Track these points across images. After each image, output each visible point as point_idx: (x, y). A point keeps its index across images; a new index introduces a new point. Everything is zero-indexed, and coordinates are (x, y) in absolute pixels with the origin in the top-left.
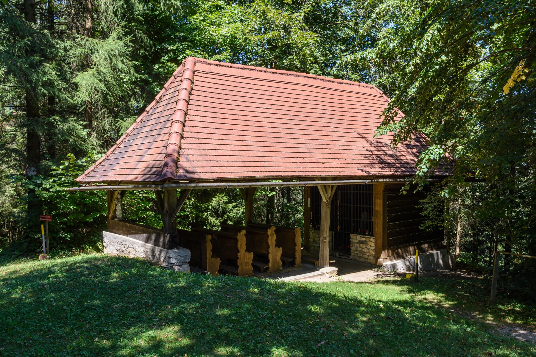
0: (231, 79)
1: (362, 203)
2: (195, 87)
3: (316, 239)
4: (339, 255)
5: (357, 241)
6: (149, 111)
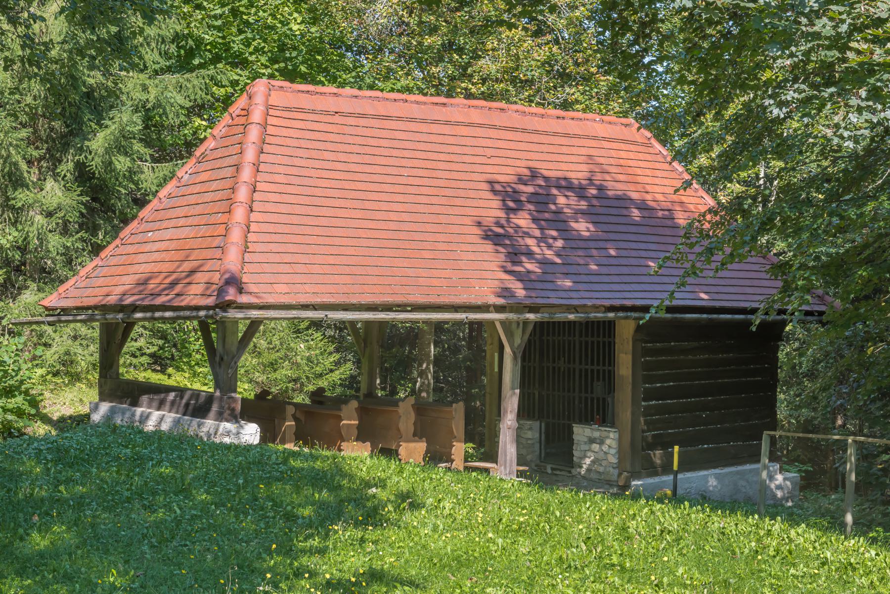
0: (337, 119)
2: (268, 139)
4: (552, 469)
6: (182, 177)
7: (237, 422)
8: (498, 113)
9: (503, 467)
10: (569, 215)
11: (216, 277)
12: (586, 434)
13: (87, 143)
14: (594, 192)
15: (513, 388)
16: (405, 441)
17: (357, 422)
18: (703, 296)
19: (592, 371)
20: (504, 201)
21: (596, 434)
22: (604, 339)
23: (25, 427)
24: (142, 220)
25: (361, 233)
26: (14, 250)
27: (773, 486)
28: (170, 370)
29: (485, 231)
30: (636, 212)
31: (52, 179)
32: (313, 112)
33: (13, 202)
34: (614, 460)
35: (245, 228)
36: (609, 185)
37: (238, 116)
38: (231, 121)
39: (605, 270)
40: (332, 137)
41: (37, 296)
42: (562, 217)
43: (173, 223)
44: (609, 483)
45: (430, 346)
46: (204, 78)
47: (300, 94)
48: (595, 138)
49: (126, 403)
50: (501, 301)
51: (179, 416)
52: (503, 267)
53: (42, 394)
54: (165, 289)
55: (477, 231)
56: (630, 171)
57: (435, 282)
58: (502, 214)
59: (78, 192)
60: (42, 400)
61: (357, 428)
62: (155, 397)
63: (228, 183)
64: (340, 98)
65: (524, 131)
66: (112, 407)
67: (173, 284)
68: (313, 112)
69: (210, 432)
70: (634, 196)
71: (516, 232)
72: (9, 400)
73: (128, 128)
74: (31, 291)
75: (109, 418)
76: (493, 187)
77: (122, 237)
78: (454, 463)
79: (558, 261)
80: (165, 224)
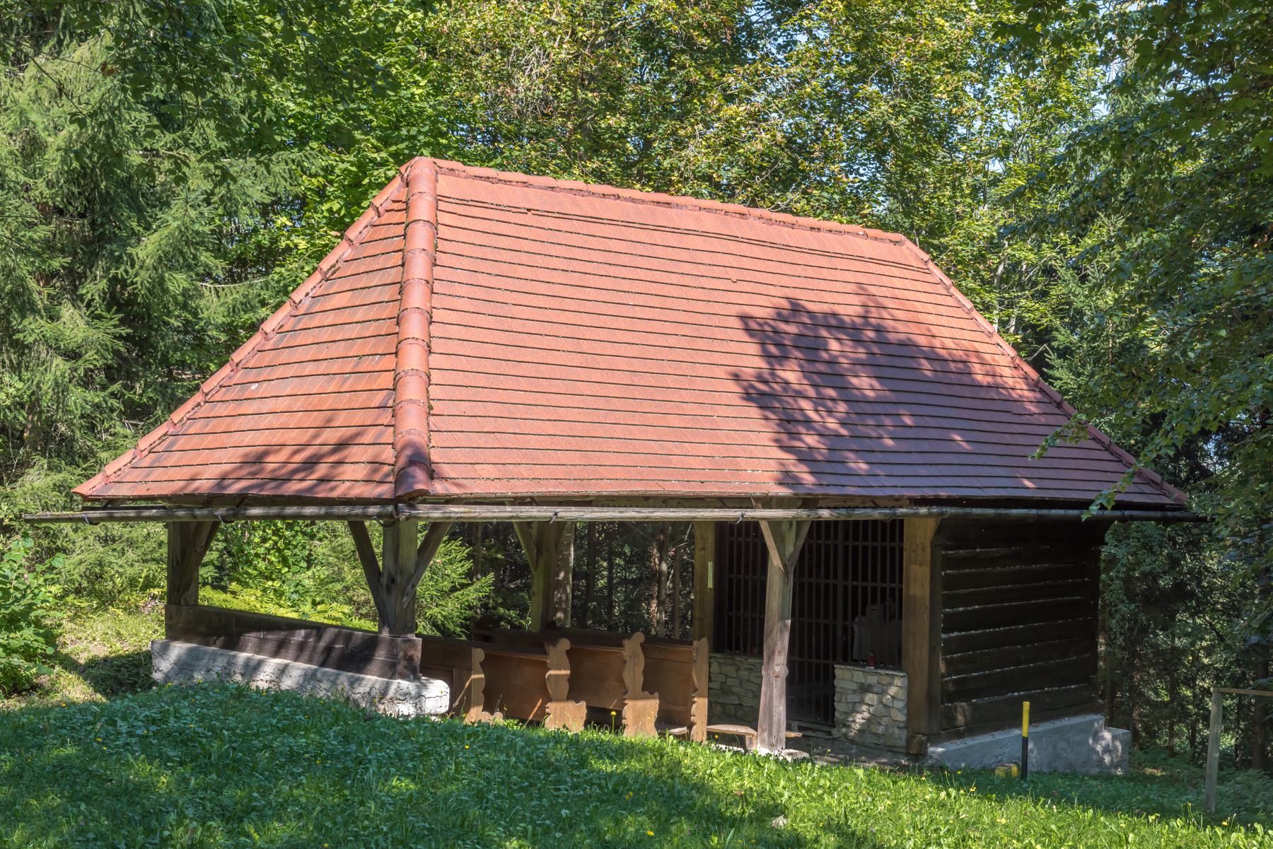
0: (529, 219)
1: (831, 587)
2: (442, 246)
3: (730, 682)
5: (855, 687)
6: (300, 302)
7: (417, 678)
8: (737, 219)
9: (766, 734)
10: (846, 366)
11: (388, 454)
12: (855, 679)
13: (129, 250)
14: (871, 334)
15: (782, 618)
16: (631, 699)
17: (568, 672)
18: (1028, 483)
19: (865, 589)
20: (763, 344)
21: (872, 680)
22: (884, 544)
23: (38, 675)
24: (237, 365)
25: (581, 388)
26: (15, 409)
27: (1099, 748)
28: (234, 586)
29: (745, 388)
30: (925, 364)
31: (70, 305)
32: (498, 207)
33: (20, 336)
34: (901, 717)
35: (425, 377)
36: (889, 324)
37: (387, 211)
38: (376, 218)
39: (904, 446)
40: (525, 246)
41: (49, 478)
42: (838, 369)
43: (292, 370)
44: (892, 750)
45: (569, 550)
46: (287, 164)
47: (477, 182)
48: (860, 258)
49: (214, 644)
50: (783, 491)
51: (314, 667)
52: (777, 441)
53: (60, 625)
54: (296, 471)
55: (733, 386)
56: (909, 305)
57: (694, 462)
58: (762, 364)
59: (115, 322)
60: (61, 634)
61: (569, 680)
62: (269, 637)
63: (390, 310)
64: (530, 190)
65: (773, 245)
66: (191, 650)
67: (310, 464)
68: (498, 207)
69: (373, 693)
70: (922, 341)
71: (785, 390)
72: (12, 635)
73: (197, 227)
74: (39, 470)
75: (184, 666)
76: (746, 324)
77: (206, 391)
78: (694, 727)
79: (844, 432)
80: (279, 372)
